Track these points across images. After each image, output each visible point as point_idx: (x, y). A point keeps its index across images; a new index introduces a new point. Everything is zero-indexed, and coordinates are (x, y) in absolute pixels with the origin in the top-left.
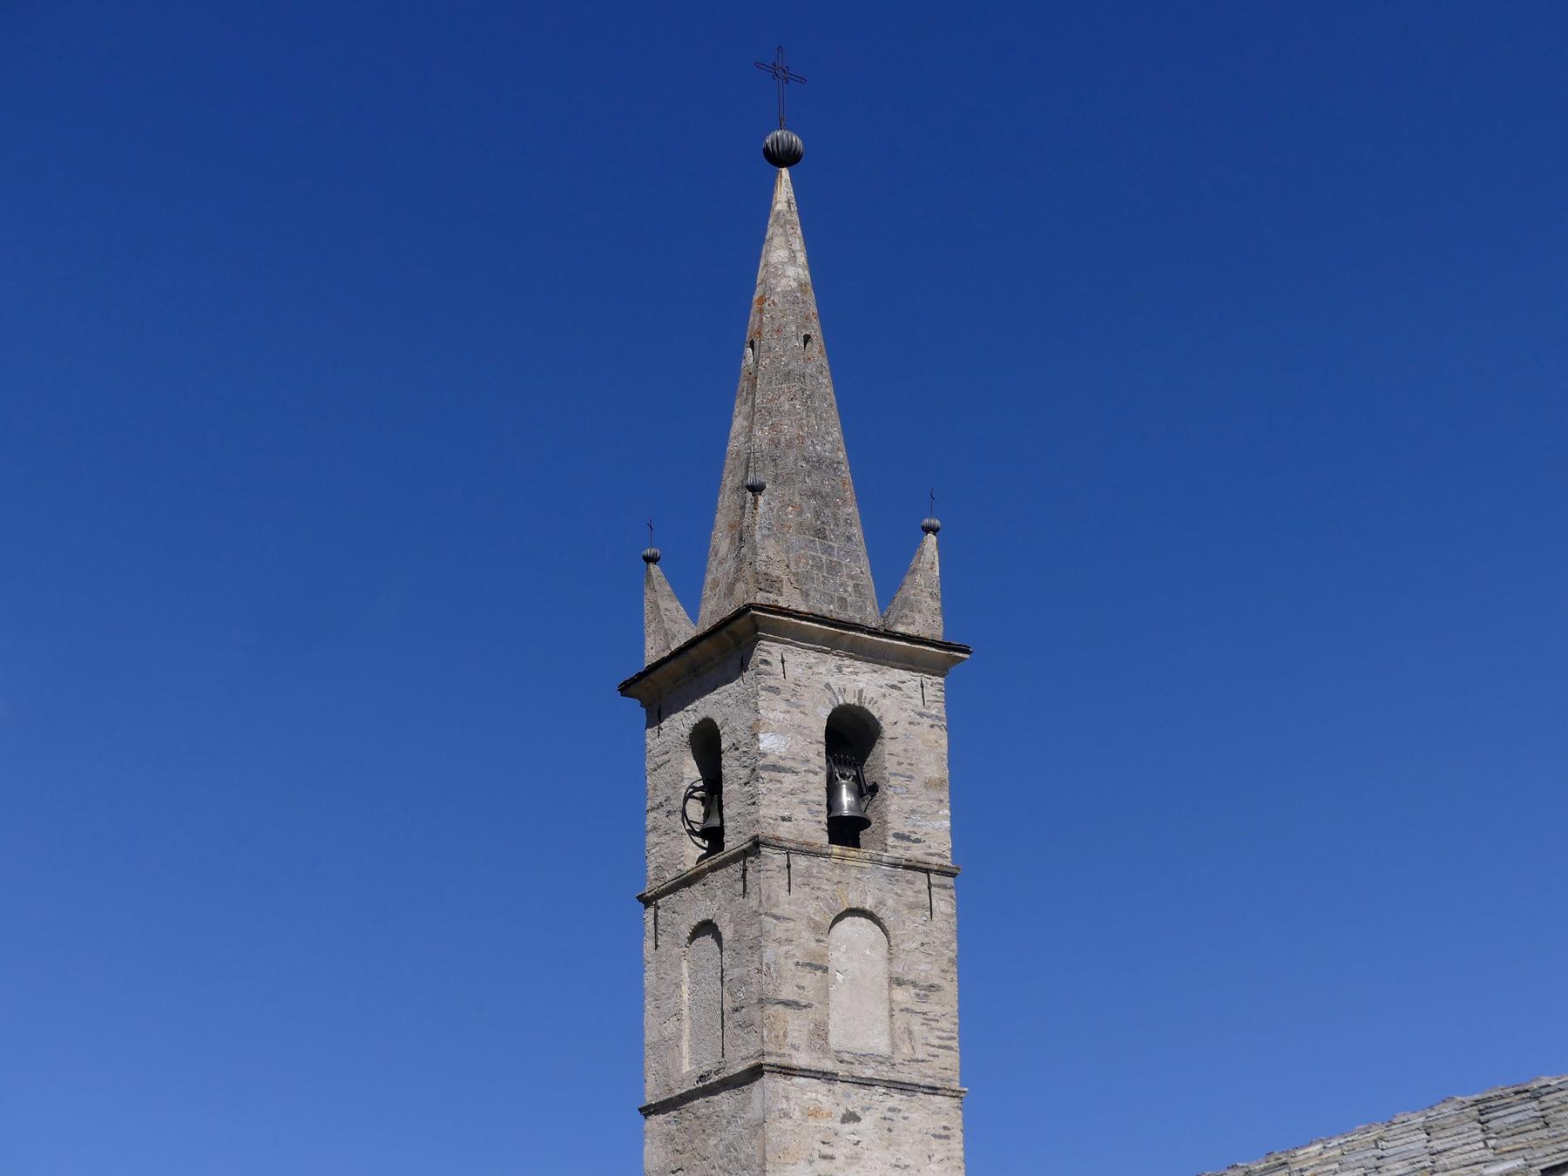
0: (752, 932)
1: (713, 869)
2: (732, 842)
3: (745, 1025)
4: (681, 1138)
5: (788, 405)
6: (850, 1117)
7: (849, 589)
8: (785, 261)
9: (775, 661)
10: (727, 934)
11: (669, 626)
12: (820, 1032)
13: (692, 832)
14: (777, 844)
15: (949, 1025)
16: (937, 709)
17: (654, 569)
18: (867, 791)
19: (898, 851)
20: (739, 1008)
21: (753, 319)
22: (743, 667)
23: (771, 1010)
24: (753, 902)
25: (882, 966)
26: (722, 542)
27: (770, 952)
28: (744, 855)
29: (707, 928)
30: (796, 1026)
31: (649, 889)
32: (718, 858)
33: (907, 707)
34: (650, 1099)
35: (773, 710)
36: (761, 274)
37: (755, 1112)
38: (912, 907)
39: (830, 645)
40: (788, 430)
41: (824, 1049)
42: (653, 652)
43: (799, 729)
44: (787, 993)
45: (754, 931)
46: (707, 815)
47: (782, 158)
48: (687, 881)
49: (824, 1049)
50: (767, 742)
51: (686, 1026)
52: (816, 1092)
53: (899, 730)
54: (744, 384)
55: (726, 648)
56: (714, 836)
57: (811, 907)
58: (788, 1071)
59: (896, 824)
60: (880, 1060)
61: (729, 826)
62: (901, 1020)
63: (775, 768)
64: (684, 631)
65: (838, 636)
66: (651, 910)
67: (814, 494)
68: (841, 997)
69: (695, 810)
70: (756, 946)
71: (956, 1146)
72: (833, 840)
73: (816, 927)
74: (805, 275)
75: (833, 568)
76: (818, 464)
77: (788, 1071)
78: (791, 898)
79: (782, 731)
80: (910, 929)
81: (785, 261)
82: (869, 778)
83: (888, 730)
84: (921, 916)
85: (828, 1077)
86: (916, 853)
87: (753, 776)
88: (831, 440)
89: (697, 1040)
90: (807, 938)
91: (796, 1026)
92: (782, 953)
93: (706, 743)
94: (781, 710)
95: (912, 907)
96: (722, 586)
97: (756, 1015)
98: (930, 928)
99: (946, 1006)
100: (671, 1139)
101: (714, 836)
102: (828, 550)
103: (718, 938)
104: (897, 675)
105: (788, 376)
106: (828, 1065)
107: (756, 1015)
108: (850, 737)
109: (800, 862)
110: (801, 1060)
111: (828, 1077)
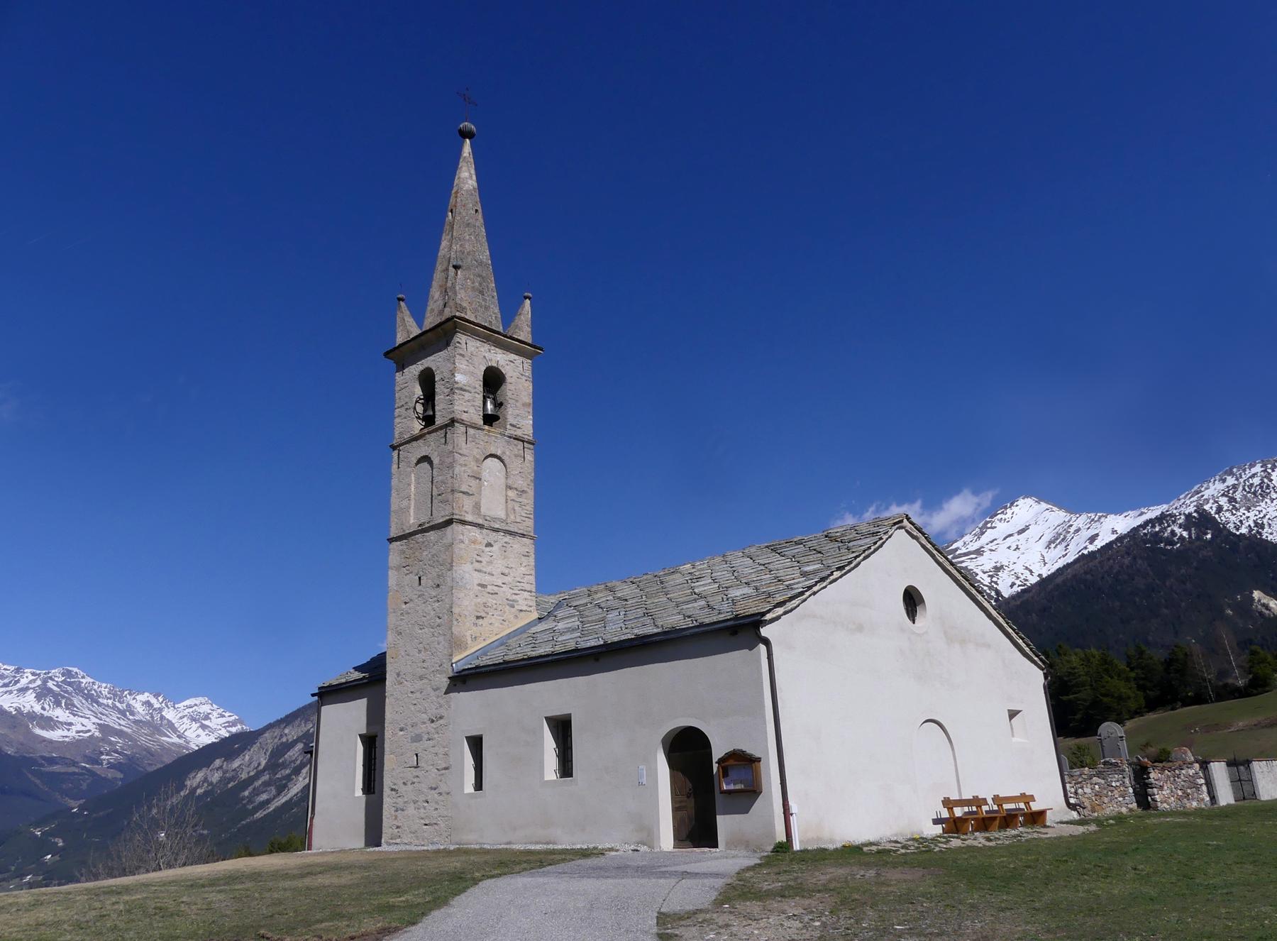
0: (449, 460)
1: (429, 433)
2: (439, 421)
3: (445, 502)
4: (408, 552)
5: (466, 236)
6: (489, 545)
7: (492, 316)
8: (467, 177)
9: (463, 342)
10: (436, 461)
11: (407, 328)
12: (477, 506)
13: (418, 418)
14: (462, 422)
15: (530, 508)
16: (529, 373)
17: (402, 303)
18: (498, 405)
19: (510, 431)
20: (439, 493)
21: (452, 200)
22: (448, 344)
23: (457, 495)
24: (450, 447)
25: (503, 480)
26: (435, 293)
27: (457, 469)
28: (446, 426)
29: (426, 459)
30: (467, 503)
31: (395, 442)
32: (431, 428)
33: (517, 370)
34: (393, 535)
35: (461, 364)
36: (456, 182)
37: (446, 541)
38: (516, 456)
39: (487, 339)
40: (468, 247)
41: (479, 515)
42: (400, 338)
43: (472, 374)
44: (464, 488)
45: (450, 460)
46: (425, 411)
47: (465, 134)
48: (415, 438)
49: (479, 515)
50: (458, 377)
51: (413, 503)
52: (474, 533)
53: (512, 380)
54: (447, 227)
55: (441, 335)
56: (429, 420)
57: (476, 452)
58: (463, 522)
59: (511, 420)
60: (502, 521)
61: (438, 414)
62: (511, 504)
63: (461, 389)
64: (416, 331)
65: (489, 336)
66: (395, 454)
67: (479, 276)
68: (486, 492)
69: (420, 408)
70: (451, 466)
71: (532, 560)
72: (485, 424)
73: (477, 460)
74: (475, 184)
75: (487, 308)
76: (481, 263)
77: (463, 522)
78: (469, 446)
79: (464, 373)
80: (515, 465)
81: (467, 177)
82: (499, 400)
83: (508, 380)
84: (520, 460)
85: (480, 526)
86: (519, 433)
87: (452, 391)
88: (485, 256)
89: (417, 509)
90: (473, 465)
91: (467, 503)
92: (463, 469)
93: (427, 379)
94: (465, 364)
95: (516, 456)
96: (436, 312)
97: (450, 497)
98: (524, 466)
99: (529, 500)
100: (403, 552)
101: (429, 420)
102: (485, 300)
103: (431, 463)
104: (513, 356)
105: (468, 225)
106: (480, 521)
107: (450, 497)
108: (493, 381)
109: (471, 431)
110: (469, 518)
111: (480, 526)
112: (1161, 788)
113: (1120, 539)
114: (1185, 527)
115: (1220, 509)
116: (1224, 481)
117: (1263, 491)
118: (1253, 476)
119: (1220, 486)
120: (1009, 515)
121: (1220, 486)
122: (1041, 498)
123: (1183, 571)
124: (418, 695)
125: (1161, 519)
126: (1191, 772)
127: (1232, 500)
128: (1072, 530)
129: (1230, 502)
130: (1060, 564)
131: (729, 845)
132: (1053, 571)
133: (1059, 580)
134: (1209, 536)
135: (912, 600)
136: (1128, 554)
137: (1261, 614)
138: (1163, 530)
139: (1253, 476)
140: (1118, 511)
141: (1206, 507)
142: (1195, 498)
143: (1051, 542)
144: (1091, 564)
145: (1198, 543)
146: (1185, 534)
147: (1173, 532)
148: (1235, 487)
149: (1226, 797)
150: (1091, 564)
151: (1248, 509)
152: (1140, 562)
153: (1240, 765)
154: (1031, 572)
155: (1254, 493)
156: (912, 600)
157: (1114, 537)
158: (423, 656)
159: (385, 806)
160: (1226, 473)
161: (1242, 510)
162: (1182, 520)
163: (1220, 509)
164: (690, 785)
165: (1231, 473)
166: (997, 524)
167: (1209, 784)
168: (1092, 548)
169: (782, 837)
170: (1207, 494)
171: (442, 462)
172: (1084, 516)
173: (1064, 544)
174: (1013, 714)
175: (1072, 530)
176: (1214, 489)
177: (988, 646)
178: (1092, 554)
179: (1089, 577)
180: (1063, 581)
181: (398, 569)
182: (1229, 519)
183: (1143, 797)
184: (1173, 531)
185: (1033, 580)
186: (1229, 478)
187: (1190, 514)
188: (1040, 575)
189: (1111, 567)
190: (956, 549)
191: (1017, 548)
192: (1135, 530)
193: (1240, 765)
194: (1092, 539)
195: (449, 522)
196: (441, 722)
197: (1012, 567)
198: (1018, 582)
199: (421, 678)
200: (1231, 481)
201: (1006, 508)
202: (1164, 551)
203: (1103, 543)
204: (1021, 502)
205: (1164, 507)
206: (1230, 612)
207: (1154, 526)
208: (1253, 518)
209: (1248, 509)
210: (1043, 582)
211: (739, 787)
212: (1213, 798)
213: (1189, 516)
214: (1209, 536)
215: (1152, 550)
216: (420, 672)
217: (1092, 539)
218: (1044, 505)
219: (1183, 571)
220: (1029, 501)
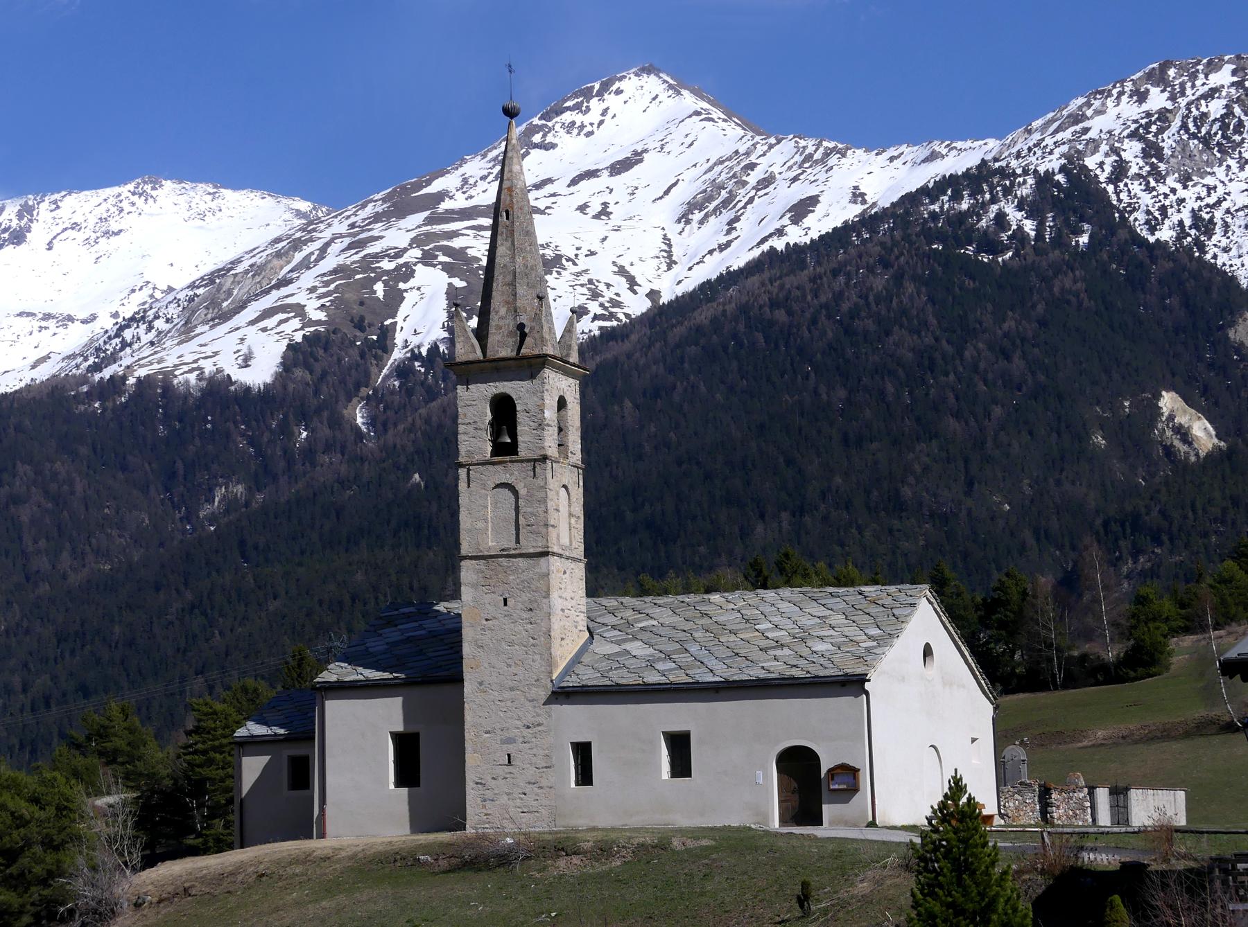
58: (554, 554)
97: (543, 530)
107: (543, 530)
112: (1058, 807)
113: (868, 221)
114: (1032, 208)
115: (1120, 171)
116: (1141, 97)
117: (1220, 141)
118: (1212, 94)
119: (1131, 110)
120: (594, 116)
121: (1131, 110)
122: (683, 79)
123: (1009, 324)
124: (509, 703)
125: (980, 178)
126: (1081, 795)
127: (1152, 151)
128: (753, 178)
129: (1146, 154)
130: (711, 269)
131: (830, 823)
132: (689, 285)
133: (703, 316)
134: (1084, 239)
135: (928, 652)
136: (886, 265)
137: (1169, 451)
138: (979, 209)
139: (1212, 94)
140: (876, 139)
141: (1091, 162)
142: (1067, 134)
143: (693, 206)
144: (790, 281)
145: (1055, 255)
146: (1029, 226)
147: (1001, 218)
148: (1164, 116)
149: (1104, 819)
150: (790, 281)
151: (1185, 180)
152: (910, 288)
153: (1119, 793)
154: (632, 283)
155: (1206, 141)
156: (928, 652)
157: (853, 212)
158: (513, 669)
159: (468, 797)
160: (1149, 77)
161: (1171, 181)
162: (1026, 189)
163: (1120, 171)
164: (795, 785)
165: (1159, 78)
166: (559, 136)
167: (1093, 807)
168: (796, 235)
169: (870, 819)
170: (1097, 126)
171: (530, 494)
172: (788, 146)
173: (727, 215)
174: (974, 740)
175: (753, 178)
176: (1115, 115)
177: (964, 686)
178: (795, 251)
179: (781, 315)
180: (714, 320)
181: (474, 586)
182: (1137, 198)
183: (1044, 812)
184: (1001, 216)
185: (637, 306)
186: (1154, 91)
187: (1049, 175)
188: (653, 295)
189: (839, 297)
190: (441, 196)
191: (604, 212)
192: (911, 200)
193: (1119, 793)
194: (800, 210)
195: (545, 554)
196: (540, 728)
197: (583, 263)
198: (594, 308)
199: (512, 689)
200: (1157, 99)
201: (588, 94)
202: (970, 268)
203: (827, 226)
204: (630, 84)
205: (988, 148)
206: (1100, 440)
207: (956, 197)
208: (1191, 204)
209: (1185, 180)
210: (663, 316)
211: (841, 787)
212: (1094, 820)
213: (1045, 180)
214: (1084, 239)
215: (946, 260)
216: (511, 684)
217: (800, 210)
218: (689, 101)
219: (1009, 324)
220: (653, 84)
